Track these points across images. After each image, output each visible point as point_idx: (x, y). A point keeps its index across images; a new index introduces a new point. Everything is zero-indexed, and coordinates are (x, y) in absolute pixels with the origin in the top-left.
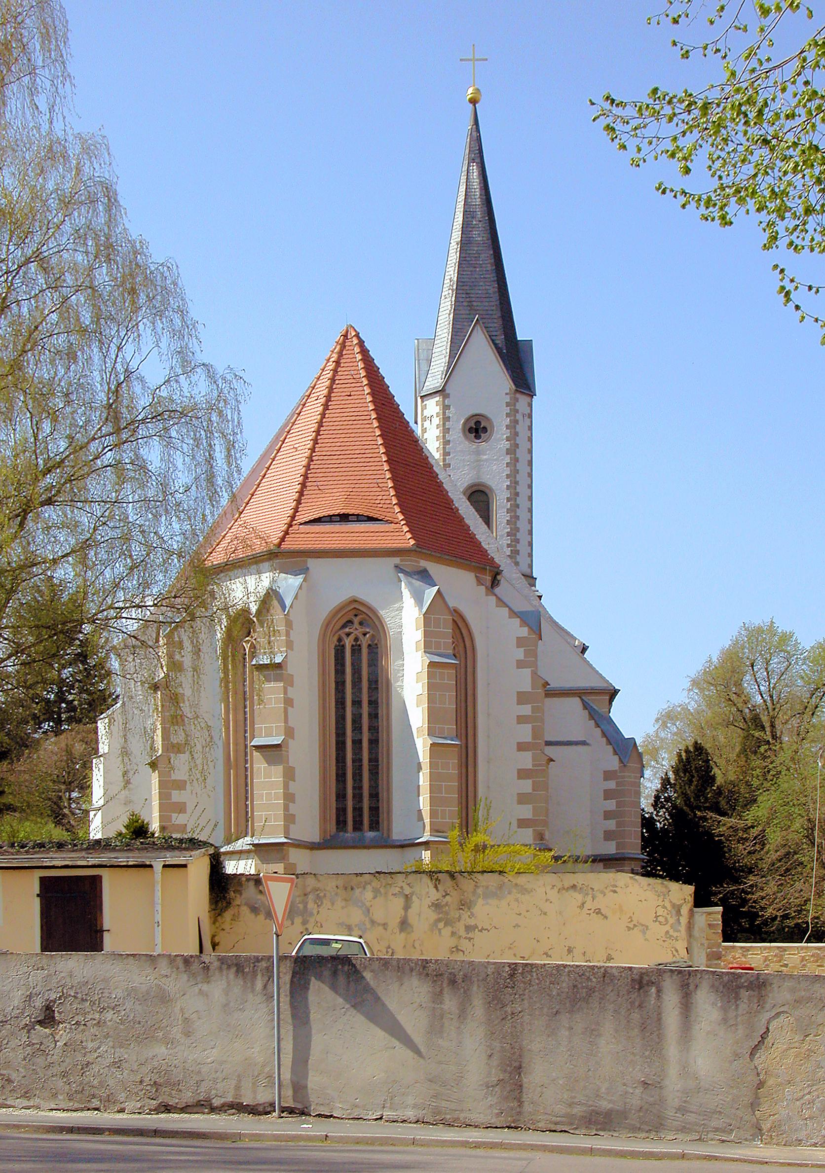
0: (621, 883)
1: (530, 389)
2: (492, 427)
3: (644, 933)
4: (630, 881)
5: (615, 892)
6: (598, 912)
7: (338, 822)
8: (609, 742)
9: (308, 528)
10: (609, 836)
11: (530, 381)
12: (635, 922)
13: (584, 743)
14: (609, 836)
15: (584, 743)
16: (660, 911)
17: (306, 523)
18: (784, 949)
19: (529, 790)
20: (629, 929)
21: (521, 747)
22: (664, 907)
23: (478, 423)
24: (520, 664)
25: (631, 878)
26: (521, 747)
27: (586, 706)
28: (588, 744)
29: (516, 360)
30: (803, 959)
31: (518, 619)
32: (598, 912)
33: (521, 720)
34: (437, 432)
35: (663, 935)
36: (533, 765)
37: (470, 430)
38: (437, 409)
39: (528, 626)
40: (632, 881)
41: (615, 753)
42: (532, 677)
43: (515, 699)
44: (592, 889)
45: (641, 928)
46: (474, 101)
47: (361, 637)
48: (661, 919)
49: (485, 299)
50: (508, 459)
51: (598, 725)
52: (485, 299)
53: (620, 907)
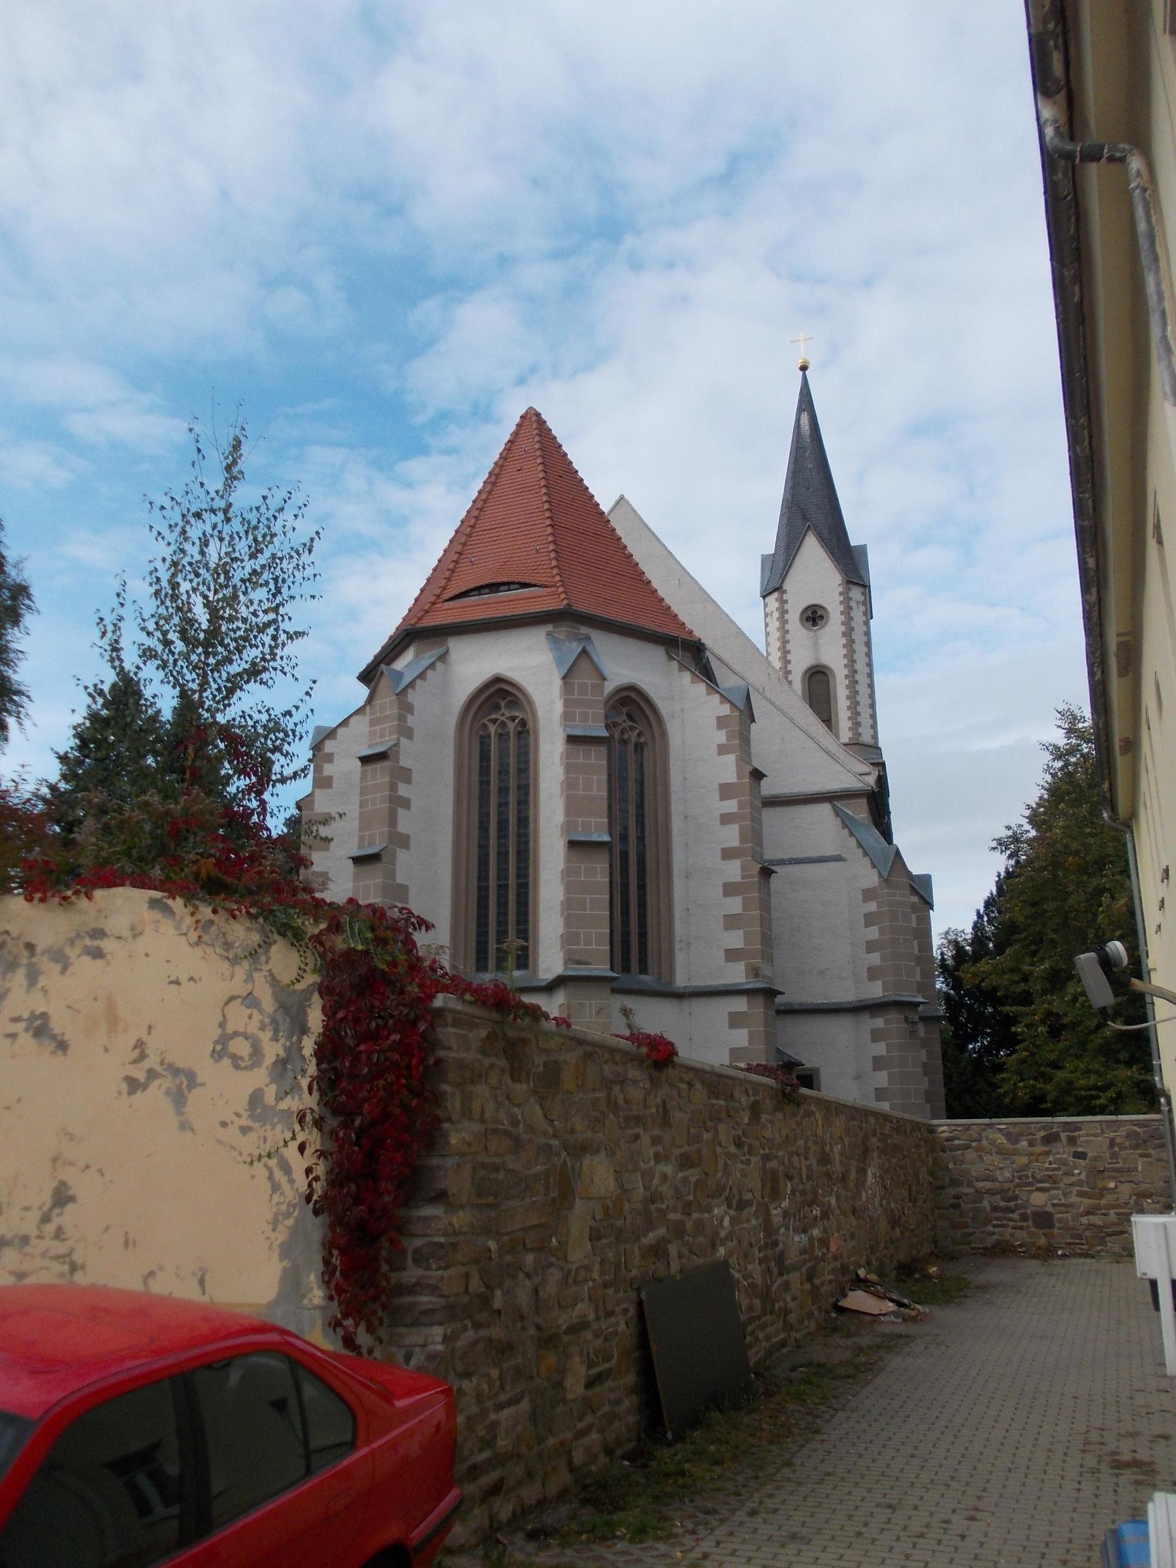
0: (119, 923)
1: (861, 578)
2: (828, 617)
3: (179, 1099)
4: (149, 915)
5: (97, 954)
6: (40, 1027)
7: (478, 960)
8: (866, 854)
9: (451, 604)
10: (873, 973)
11: (863, 574)
12: (152, 1062)
13: (838, 859)
14: (873, 973)
15: (838, 859)
16: (239, 1017)
17: (451, 599)
18: (1077, 1127)
19: (739, 910)
20: (134, 1085)
21: (727, 854)
22: (250, 1000)
23: (814, 612)
24: (722, 750)
25: (153, 903)
26: (727, 854)
27: (837, 813)
28: (844, 860)
29: (851, 564)
30: (1112, 1143)
31: (718, 696)
32: (40, 1027)
33: (726, 819)
34: (777, 624)
35: (242, 1105)
36: (743, 877)
37: (808, 619)
38: (777, 605)
39: (729, 701)
40: (156, 915)
41: (874, 866)
42: (737, 766)
43: (717, 794)
44: (30, 947)
45: (167, 1082)
46: (804, 368)
47: (508, 722)
48: (242, 1048)
49: (811, 504)
50: (844, 641)
51: (852, 834)
52: (811, 504)
53: (111, 1006)
